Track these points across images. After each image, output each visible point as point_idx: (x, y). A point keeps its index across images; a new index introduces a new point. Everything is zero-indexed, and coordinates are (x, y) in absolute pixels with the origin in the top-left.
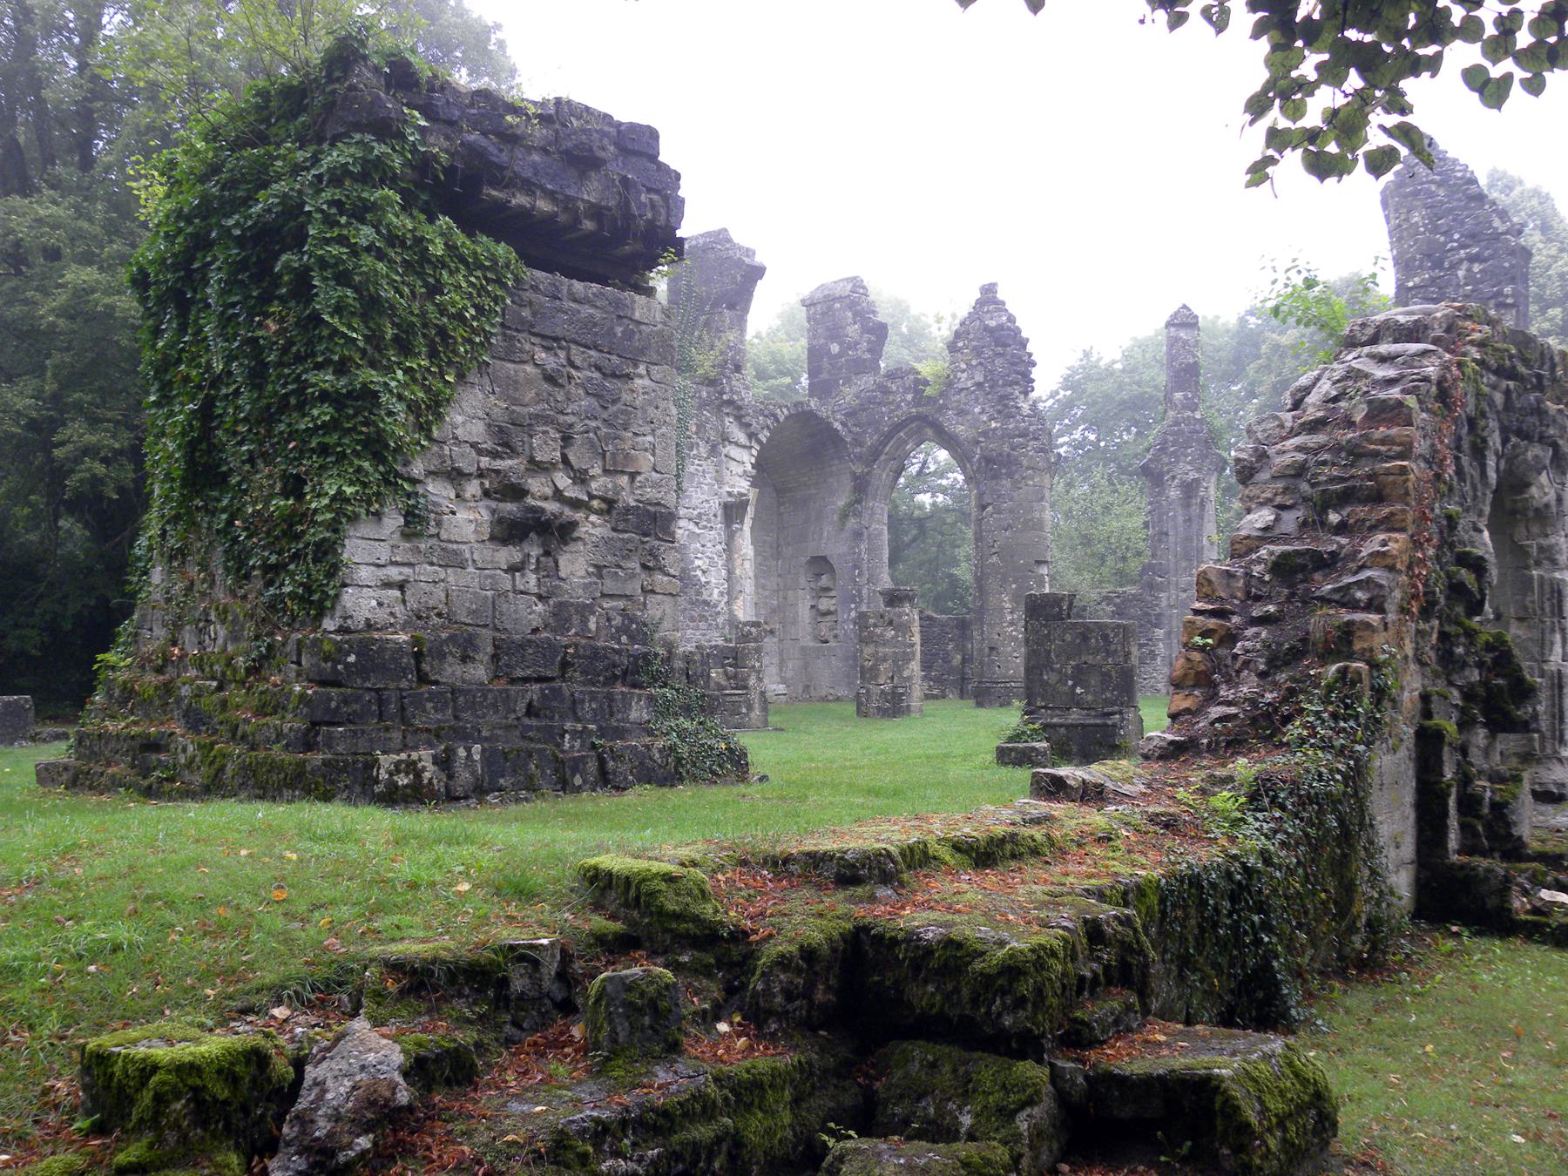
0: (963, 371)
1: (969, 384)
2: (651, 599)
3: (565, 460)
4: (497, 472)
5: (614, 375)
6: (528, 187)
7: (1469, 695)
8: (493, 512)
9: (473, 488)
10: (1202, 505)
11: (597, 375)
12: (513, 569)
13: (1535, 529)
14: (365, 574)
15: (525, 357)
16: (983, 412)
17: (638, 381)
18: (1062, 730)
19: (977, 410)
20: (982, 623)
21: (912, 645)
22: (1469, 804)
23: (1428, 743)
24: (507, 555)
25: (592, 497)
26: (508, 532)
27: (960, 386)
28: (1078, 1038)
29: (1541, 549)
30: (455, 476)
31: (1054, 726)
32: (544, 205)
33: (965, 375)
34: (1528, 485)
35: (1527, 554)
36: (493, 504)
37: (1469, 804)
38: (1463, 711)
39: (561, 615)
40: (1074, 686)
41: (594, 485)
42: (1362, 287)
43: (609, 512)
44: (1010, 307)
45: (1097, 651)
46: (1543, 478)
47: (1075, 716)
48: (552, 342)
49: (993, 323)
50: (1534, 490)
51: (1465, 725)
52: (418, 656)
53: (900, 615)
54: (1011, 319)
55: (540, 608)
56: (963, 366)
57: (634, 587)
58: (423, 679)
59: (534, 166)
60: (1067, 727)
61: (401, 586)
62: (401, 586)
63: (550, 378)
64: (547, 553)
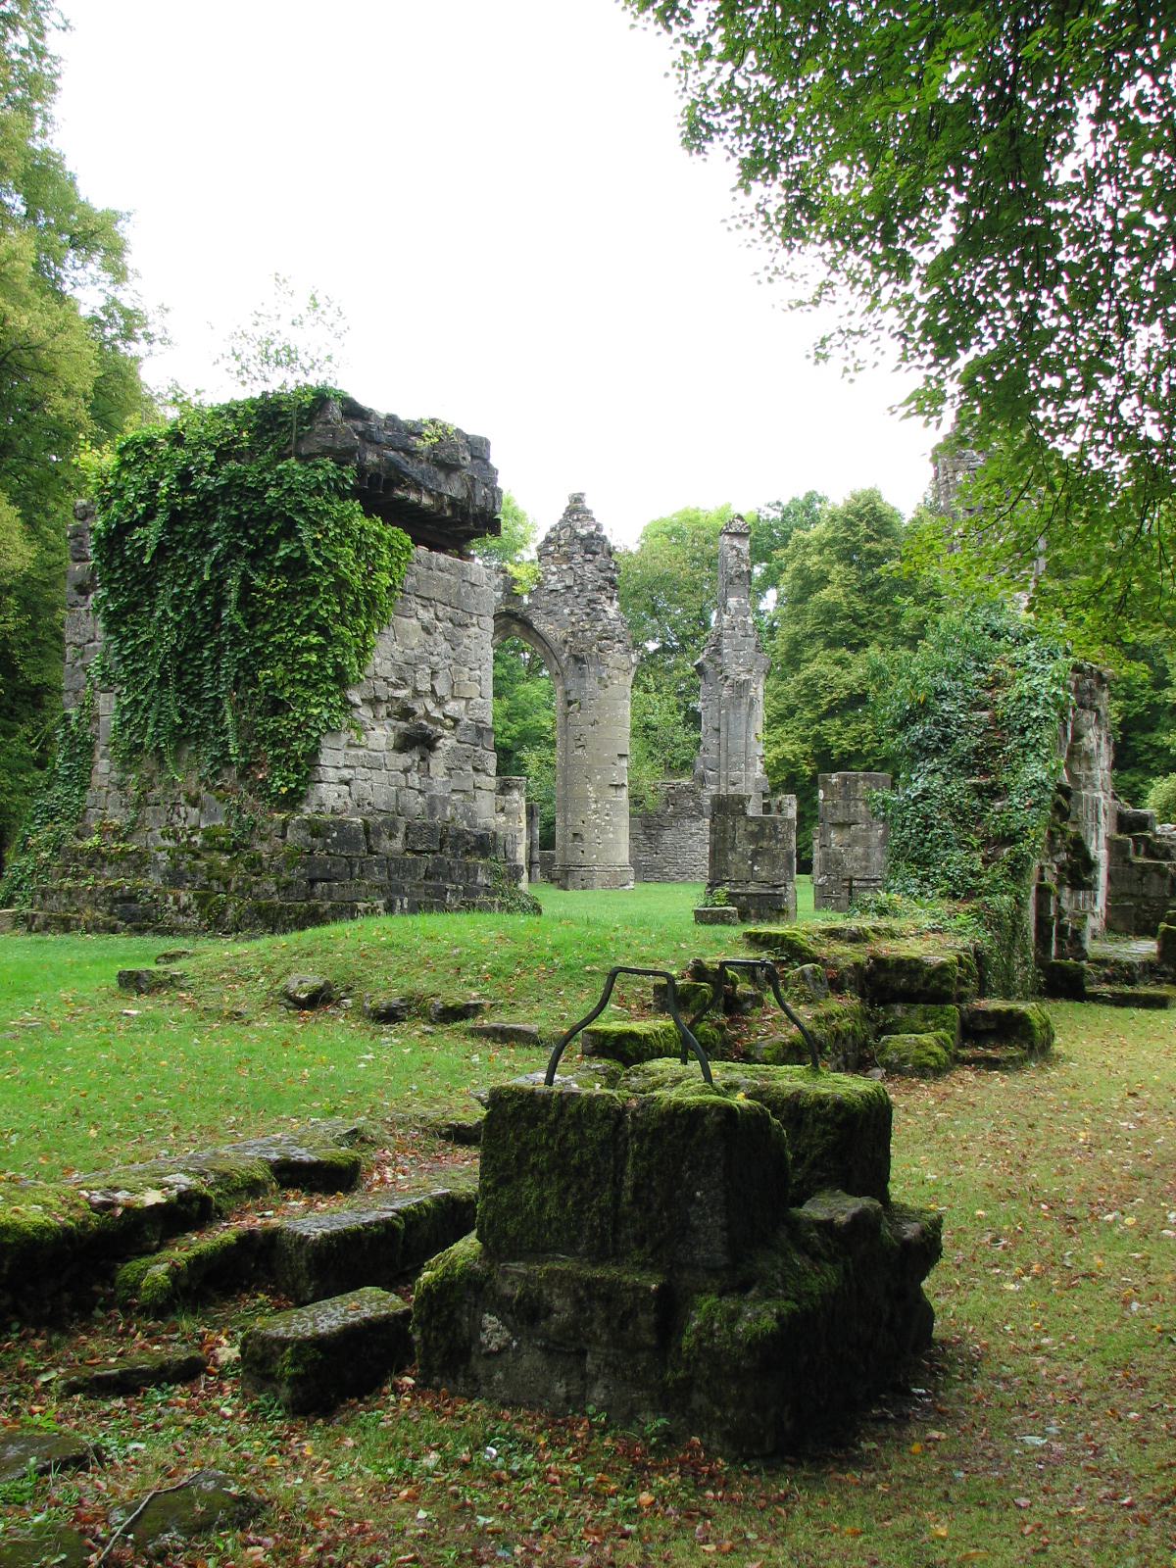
0: (554, 574)
1: (559, 586)
2: (479, 793)
3: (433, 691)
4: (397, 699)
5: (460, 625)
6: (418, 487)
7: (1061, 868)
8: (394, 728)
9: (382, 711)
10: (751, 705)
11: (450, 625)
12: (406, 771)
13: (1084, 765)
14: (331, 774)
15: (412, 613)
16: (572, 613)
17: (472, 629)
18: (743, 898)
19: (567, 611)
20: (565, 810)
21: (521, 830)
22: (1062, 930)
23: (1043, 891)
24: (405, 760)
25: (446, 716)
26: (404, 744)
27: (551, 587)
28: (961, 998)
29: (1087, 777)
30: (374, 702)
31: (738, 895)
32: (426, 501)
33: (556, 577)
34: (1082, 736)
35: (1079, 781)
36: (394, 722)
37: (1062, 930)
38: (1059, 877)
39: (431, 807)
40: (752, 865)
41: (447, 708)
42: (895, 514)
43: (454, 728)
44: (597, 516)
45: (770, 838)
46: (1090, 732)
47: (752, 889)
48: (428, 601)
49: (583, 532)
50: (1085, 740)
51: (1060, 884)
52: (367, 832)
53: (510, 802)
54: (599, 528)
55: (420, 799)
56: (554, 569)
57: (468, 785)
58: (371, 852)
59: (422, 472)
60: (747, 895)
61: (347, 783)
62: (347, 783)
63: (426, 630)
64: (423, 759)
